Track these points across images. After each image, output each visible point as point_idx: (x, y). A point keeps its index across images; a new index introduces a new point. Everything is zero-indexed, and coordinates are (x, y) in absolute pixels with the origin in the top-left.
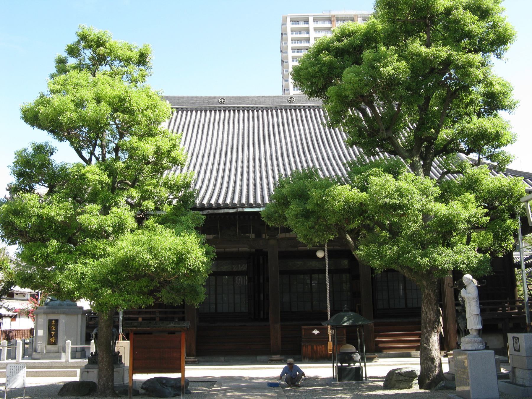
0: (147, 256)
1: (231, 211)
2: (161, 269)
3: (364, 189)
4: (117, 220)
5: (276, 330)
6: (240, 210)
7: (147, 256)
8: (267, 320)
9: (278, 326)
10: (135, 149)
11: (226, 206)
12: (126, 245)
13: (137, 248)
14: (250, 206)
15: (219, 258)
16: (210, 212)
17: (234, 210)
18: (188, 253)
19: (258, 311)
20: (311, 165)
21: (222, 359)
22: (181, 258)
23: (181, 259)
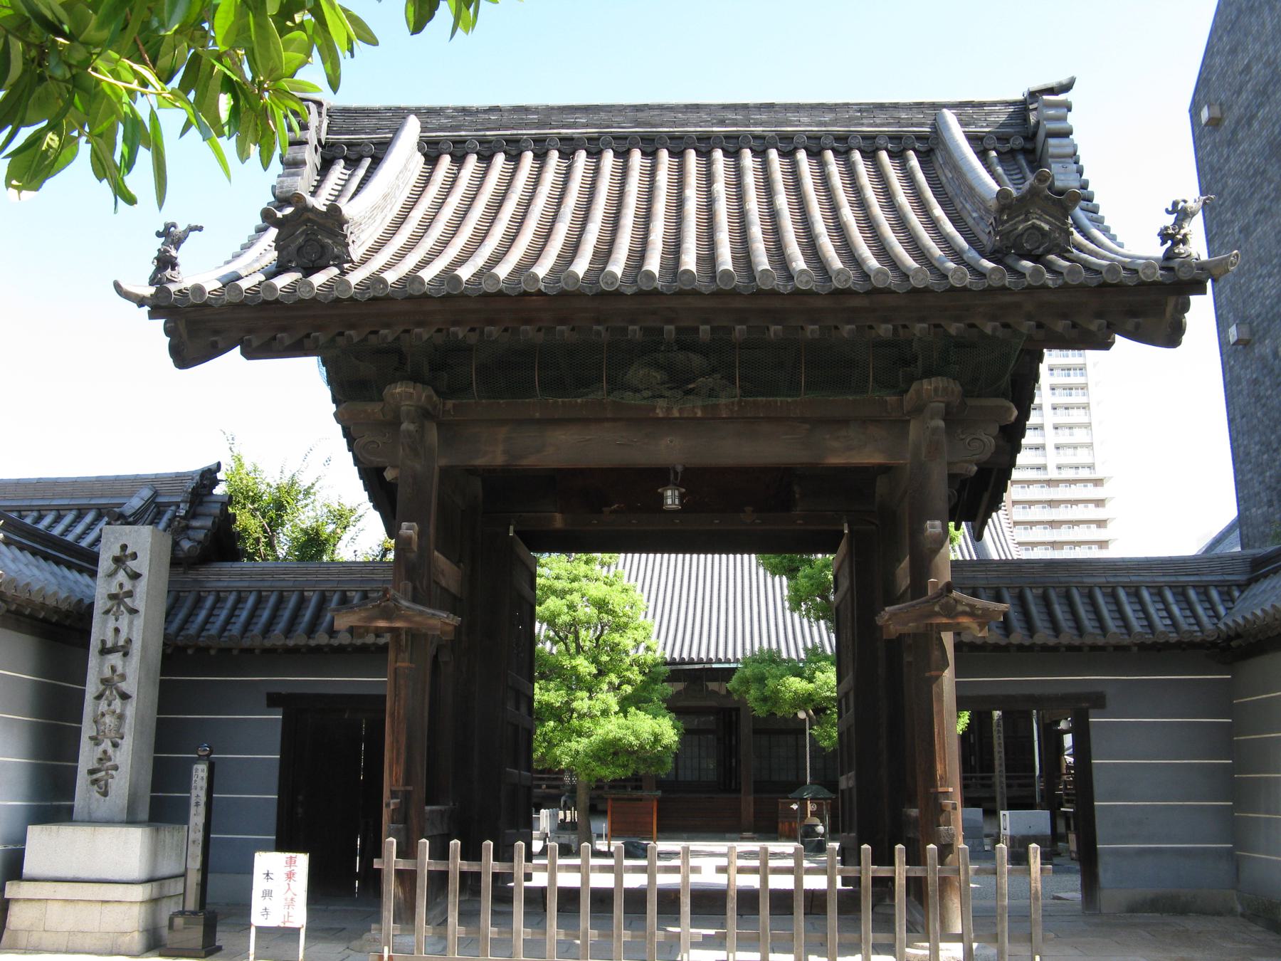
0: (632, 738)
1: (697, 667)
2: (642, 747)
3: (811, 680)
4: (604, 707)
5: (748, 803)
6: (707, 666)
7: (632, 738)
8: (739, 791)
9: (751, 798)
10: (618, 645)
11: (691, 662)
12: (612, 728)
13: (624, 731)
14: (719, 661)
15: (687, 735)
16: (674, 667)
17: (701, 666)
18: (662, 734)
19: (728, 781)
20: (774, 646)
21: (685, 835)
22: (657, 738)
23: (657, 738)
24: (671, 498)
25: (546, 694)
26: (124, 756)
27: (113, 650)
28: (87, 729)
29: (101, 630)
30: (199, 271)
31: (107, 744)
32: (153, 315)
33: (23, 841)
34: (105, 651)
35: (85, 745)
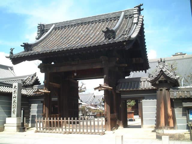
24: (75, 74)
25: (80, 102)
26: (16, 110)
27: (15, 97)
28: (12, 107)
29: (13, 95)
30: (15, 52)
31: (14, 108)
32: (10, 59)
33: (6, 119)
34: (14, 98)
35: (12, 108)
